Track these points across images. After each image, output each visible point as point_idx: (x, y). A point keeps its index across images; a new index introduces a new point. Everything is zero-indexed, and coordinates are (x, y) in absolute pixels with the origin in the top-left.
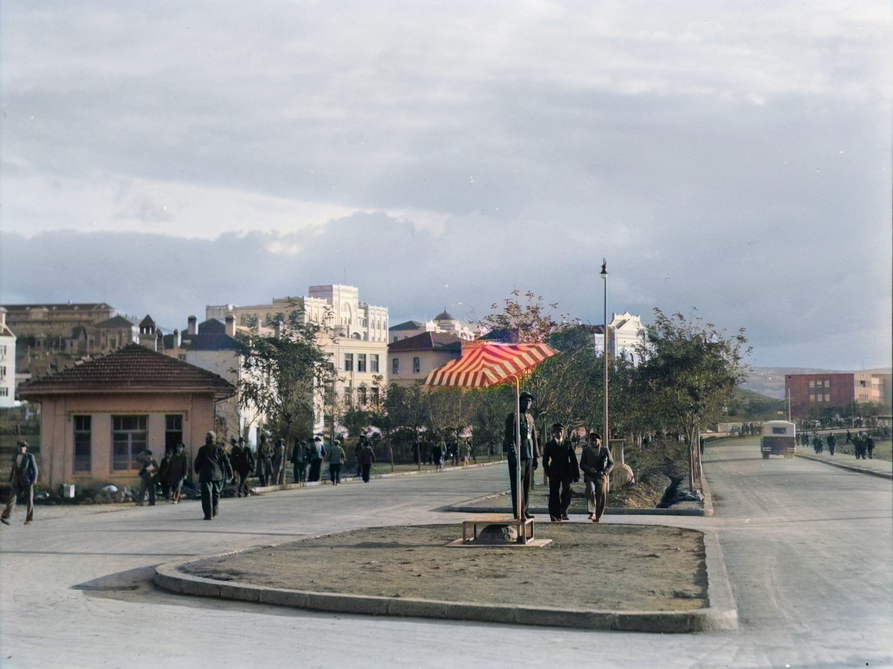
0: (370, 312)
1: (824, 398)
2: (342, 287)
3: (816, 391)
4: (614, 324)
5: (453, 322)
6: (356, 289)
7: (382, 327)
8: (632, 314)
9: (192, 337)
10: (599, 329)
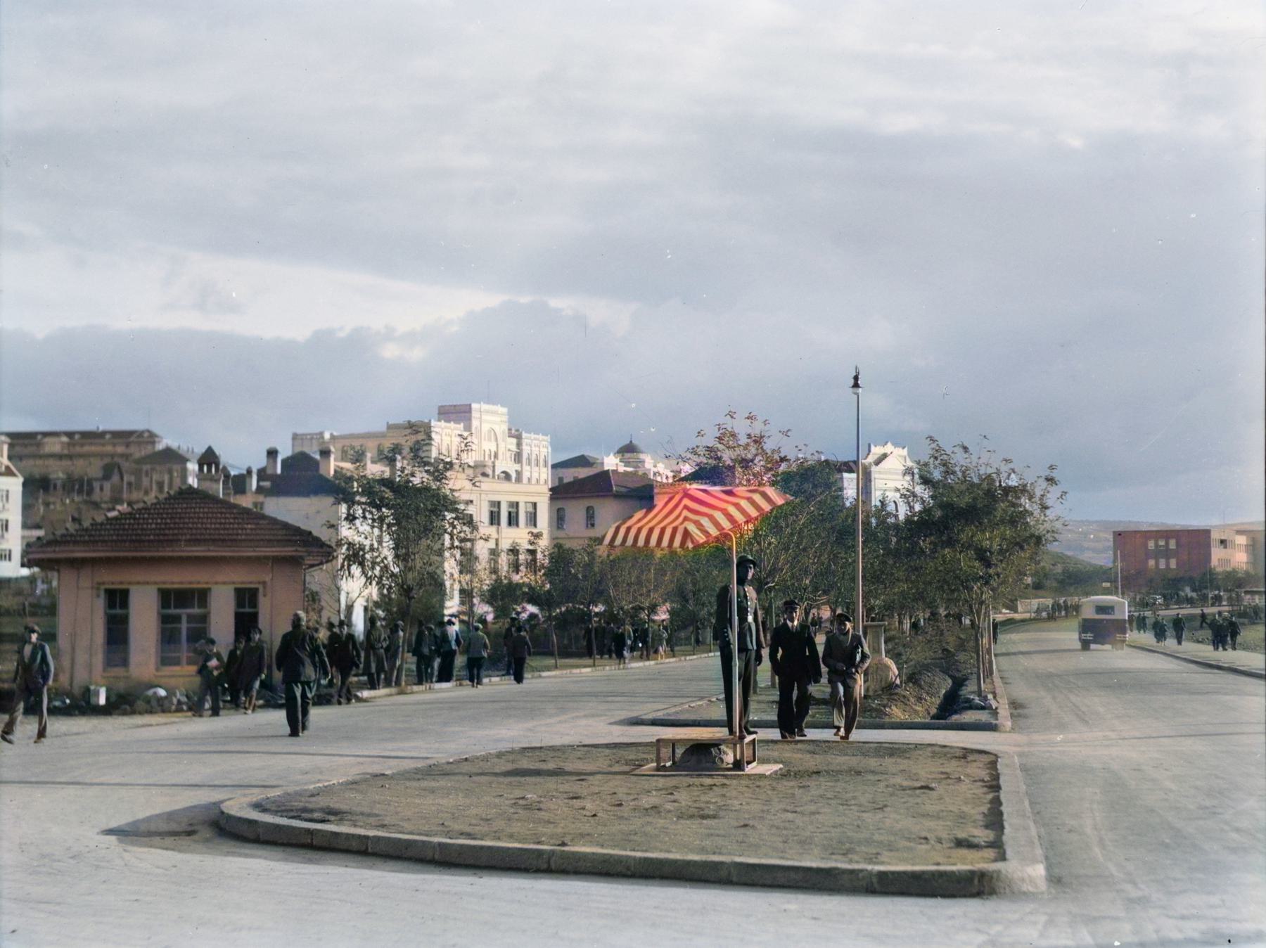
0: (525, 442)
1: (1168, 564)
2: (485, 407)
3: (1157, 554)
4: (871, 459)
5: (642, 456)
6: (505, 410)
7: (542, 463)
8: (896, 445)
9: (273, 478)
10: (849, 467)
